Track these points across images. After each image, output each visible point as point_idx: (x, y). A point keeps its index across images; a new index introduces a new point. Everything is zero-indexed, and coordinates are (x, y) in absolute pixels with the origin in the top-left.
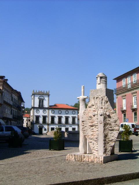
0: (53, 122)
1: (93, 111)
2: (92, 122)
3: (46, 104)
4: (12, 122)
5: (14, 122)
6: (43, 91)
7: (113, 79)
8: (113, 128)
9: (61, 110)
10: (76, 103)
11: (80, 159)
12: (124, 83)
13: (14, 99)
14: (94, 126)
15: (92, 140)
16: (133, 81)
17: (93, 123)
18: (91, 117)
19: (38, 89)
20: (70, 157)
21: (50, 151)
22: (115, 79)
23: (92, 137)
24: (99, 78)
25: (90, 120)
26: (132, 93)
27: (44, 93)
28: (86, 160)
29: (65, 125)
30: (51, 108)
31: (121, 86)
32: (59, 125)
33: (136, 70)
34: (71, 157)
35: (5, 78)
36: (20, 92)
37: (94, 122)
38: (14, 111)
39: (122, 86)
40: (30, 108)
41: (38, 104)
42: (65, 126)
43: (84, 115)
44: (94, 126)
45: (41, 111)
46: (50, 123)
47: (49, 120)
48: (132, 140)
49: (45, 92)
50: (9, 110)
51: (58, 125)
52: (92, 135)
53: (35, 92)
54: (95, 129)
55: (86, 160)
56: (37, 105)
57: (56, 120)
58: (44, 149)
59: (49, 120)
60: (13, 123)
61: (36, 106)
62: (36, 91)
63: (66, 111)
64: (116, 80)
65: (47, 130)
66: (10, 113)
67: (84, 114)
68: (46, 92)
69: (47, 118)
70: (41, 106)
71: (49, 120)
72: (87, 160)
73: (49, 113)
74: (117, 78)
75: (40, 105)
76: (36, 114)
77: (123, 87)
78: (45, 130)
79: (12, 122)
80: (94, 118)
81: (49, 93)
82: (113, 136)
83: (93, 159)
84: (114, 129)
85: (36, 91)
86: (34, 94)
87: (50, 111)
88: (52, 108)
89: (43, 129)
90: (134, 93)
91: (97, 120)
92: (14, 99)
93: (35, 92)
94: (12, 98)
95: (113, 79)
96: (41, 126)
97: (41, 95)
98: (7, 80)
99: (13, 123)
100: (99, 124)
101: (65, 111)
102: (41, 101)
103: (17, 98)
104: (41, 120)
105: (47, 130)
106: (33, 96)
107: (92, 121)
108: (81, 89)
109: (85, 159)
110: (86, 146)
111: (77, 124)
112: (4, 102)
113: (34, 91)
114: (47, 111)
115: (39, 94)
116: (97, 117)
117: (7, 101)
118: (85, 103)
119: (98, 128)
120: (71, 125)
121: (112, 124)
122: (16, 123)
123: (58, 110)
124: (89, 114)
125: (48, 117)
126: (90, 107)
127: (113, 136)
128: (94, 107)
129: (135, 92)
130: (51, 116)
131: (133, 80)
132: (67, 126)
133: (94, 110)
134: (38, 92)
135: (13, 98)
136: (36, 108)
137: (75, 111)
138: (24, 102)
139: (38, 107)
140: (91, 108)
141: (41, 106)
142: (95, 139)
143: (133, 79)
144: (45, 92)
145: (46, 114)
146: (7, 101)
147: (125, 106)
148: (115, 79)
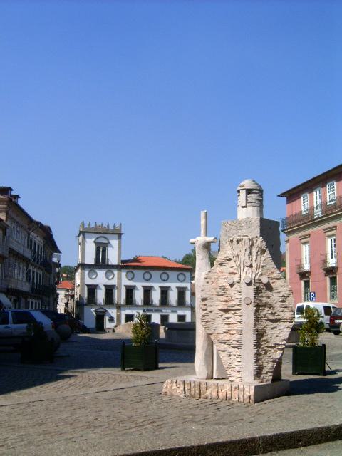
1: (230, 273)
2: (226, 301)
3: (113, 257)
4: (30, 300)
5: (34, 301)
6: (105, 225)
7: (279, 196)
8: (279, 315)
9: (150, 272)
10: (188, 253)
11: (197, 392)
12: (304, 206)
13: (35, 244)
14: (232, 310)
15: (226, 346)
16: (328, 200)
17: (230, 303)
18: (223, 289)
19: (93, 220)
20: (173, 388)
21: (123, 373)
22: (282, 195)
23: (227, 337)
24: (244, 191)
25: (222, 295)
26: (324, 230)
27: (108, 229)
28: (211, 394)
29: (159, 308)
30: (125, 266)
31: (298, 211)
32: (146, 308)
33: (334, 172)
34: (174, 387)
35: (13, 193)
36: (49, 227)
37: (231, 301)
38: (33, 272)
39: (301, 212)
40: (73, 266)
41: (94, 256)
42: (161, 311)
43: (208, 282)
44: (232, 310)
45: (101, 274)
46: (123, 302)
47: (120, 296)
49: (111, 227)
51: (143, 308)
52: (227, 333)
53: (86, 226)
54: (234, 319)
55: (211, 394)
57: (139, 296)
58: (109, 367)
59: (119, 296)
60: (32, 303)
61: (88, 261)
62: (90, 225)
63: (162, 274)
64: (285, 198)
65: (115, 320)
66: (24, 280)
67: (207, 280)
68: (114, 226)
69: (116, 292)
70: (101, 262)
71: (120, 296)
72: (215, 394)
73: (120, 278)
74: (288, 192)
75: (97, 259)
76: (88, 281)
77: (303, 214)
78: (111, 320)
79: (30, 300)
80: (232, 291)
81: (120, 230)
82: (277, 336)
83: (229, 392)
84: (280, 317)
85: (90, 225)
86: (83, 233)
87: (124, 274)
88: (128, 266)
89: (107, 318)
90: (329, 228)
91: (238, 296)
92: (35, 244)
93: (86, 226)
94: (30, 241)
95: (279, 196)
96: (101, 310)
97: (100, 233)
98: (17, 197)
99: (32, 303)
100: (243, 306)
101: (159, 273)
102: (101, 250)
103: (42, 241)
104: (101, 296)
105: (115, 320)
106: (81, 237)
107: (226, 299)
108: (200, 220)
109: (208, 392)
110: (211, 359)
111: (188, 307)
112: (9, 252)
113: (83, 224)
114: (116, 272)
115: (97, 233)
116: (238, 289)
117: (17, 249)
118: (210, 254)
119: (240, 316)
120: (174, 309)
121: (275, 305)
122: (39, 304)
123: (144, 271)
124: (219, 282)
125: (117, 288)
126: (221, 264)
127: (277, 336)
128: (232, 263)
129: (333, 227)
130: (126, 286)
131: (328, 197)
132: (166, 311)
133: (232, 270)
134: (93, 226)
135: (31, 241)
136: (89, 266)
137: (185, 273)
138: (60, 252)
139: (93, 263)
140: (223, 267)
141: (101, 262)
142: (235, 342)
143: (328, 194)
144: (111, 227)
145: (114, 282)
146: (17, 249)
147: (308, 261)
148: (282, 195)
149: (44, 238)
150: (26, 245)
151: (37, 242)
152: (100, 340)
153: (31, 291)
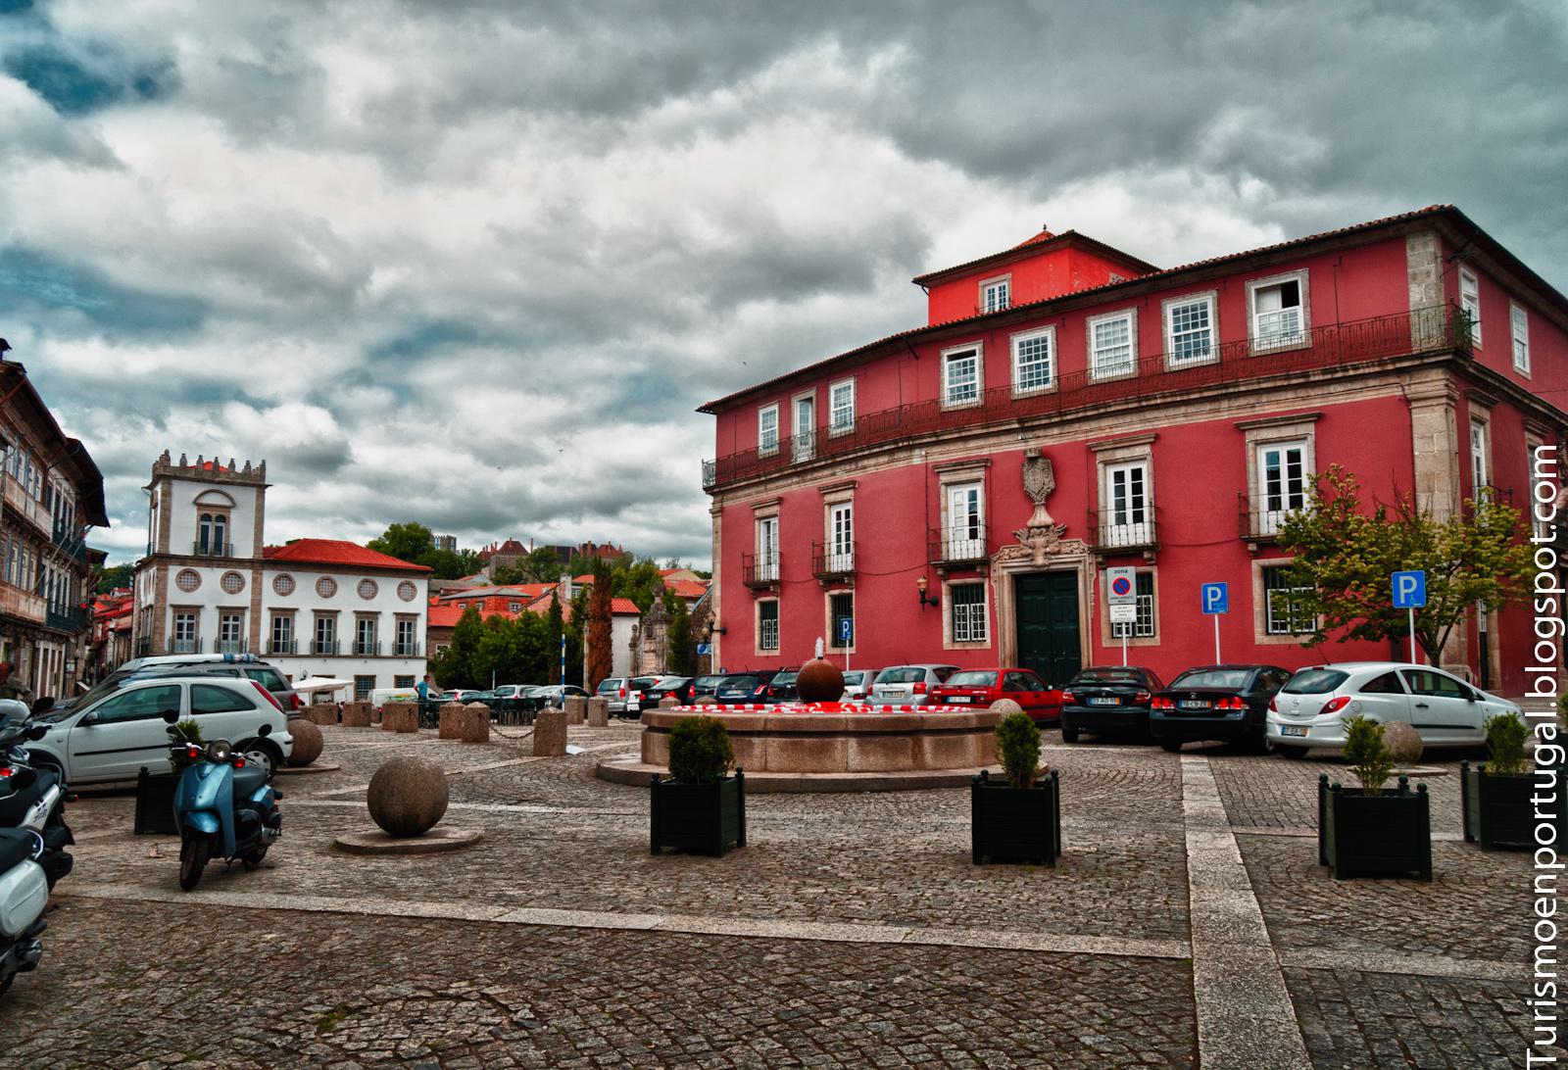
0: (324, 646)
4: (42, 645)
5: (51, 646)
6: (224, 464)
9: (292, 574)
16: (832, 422)
26: (820, 489)
31: (748, 447)
38: (52, 571)
39: (936, 401)
45: (211, 578)
48: (1055, 774)
49: (240, 468)
50: (25, 570)
56: (182, 543)
59: (255, 634)
60: (46, 650)
61: (175, 549)
63: (401, 585)
64: (715, 417)
70: (212, 551)
75: (202, 543)
76: (176, 595)
79: (42, 645)
81: (262, 476)
87: (268, 577)
90: (836, 486)
93: (175, 462)
94: (47, 489)
99: (46, 650)
102: (214, 521)
106: (159, 489)
110: (126, 713)
113: (166, 456)
117: (22, 507)
122: (60, 653)
123: (319, 576)
129: (846, 484)
130: (272, 610)
134: (192, 462)
135: (50, 489)
136: (180, 560)
141: (212, 551)
144: (240, 468)
145: (243, 599)
146: (22, 507)
147: (775, 557)
148: (707, 409)
149: (1472, 347)
150: (39, 499)
151: (64, 494)
152: (615, 771)
153: (44, 621)
